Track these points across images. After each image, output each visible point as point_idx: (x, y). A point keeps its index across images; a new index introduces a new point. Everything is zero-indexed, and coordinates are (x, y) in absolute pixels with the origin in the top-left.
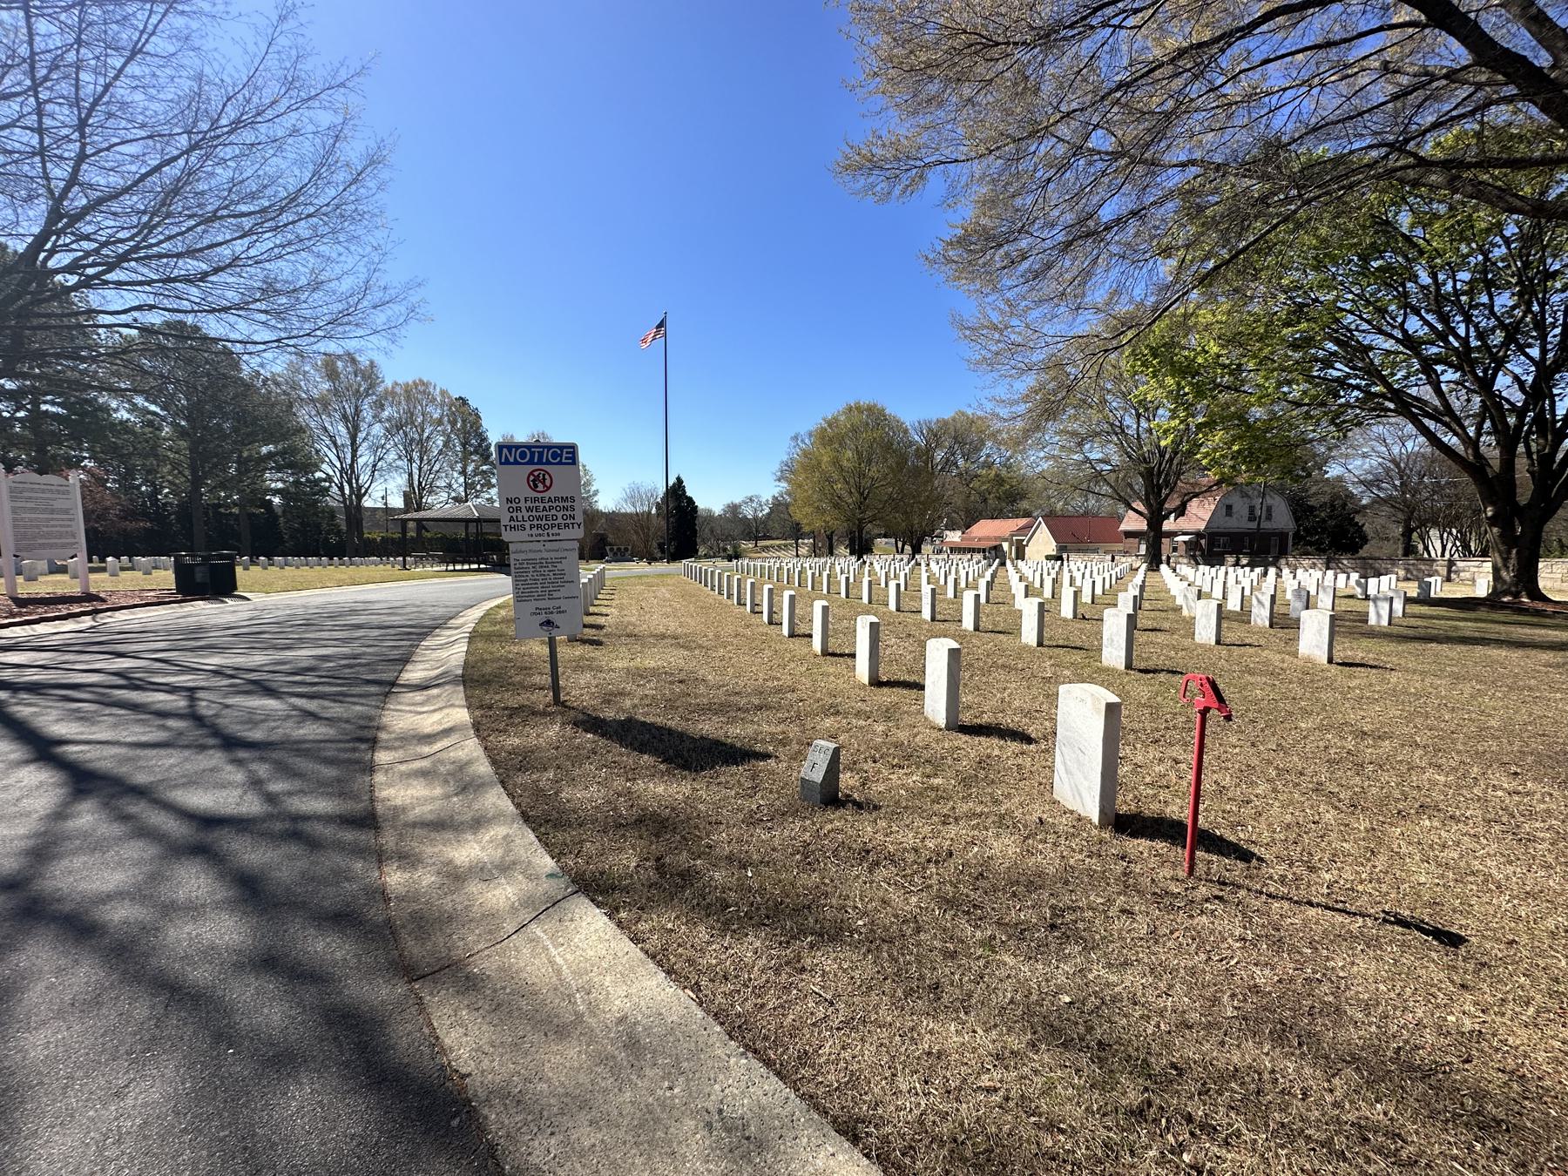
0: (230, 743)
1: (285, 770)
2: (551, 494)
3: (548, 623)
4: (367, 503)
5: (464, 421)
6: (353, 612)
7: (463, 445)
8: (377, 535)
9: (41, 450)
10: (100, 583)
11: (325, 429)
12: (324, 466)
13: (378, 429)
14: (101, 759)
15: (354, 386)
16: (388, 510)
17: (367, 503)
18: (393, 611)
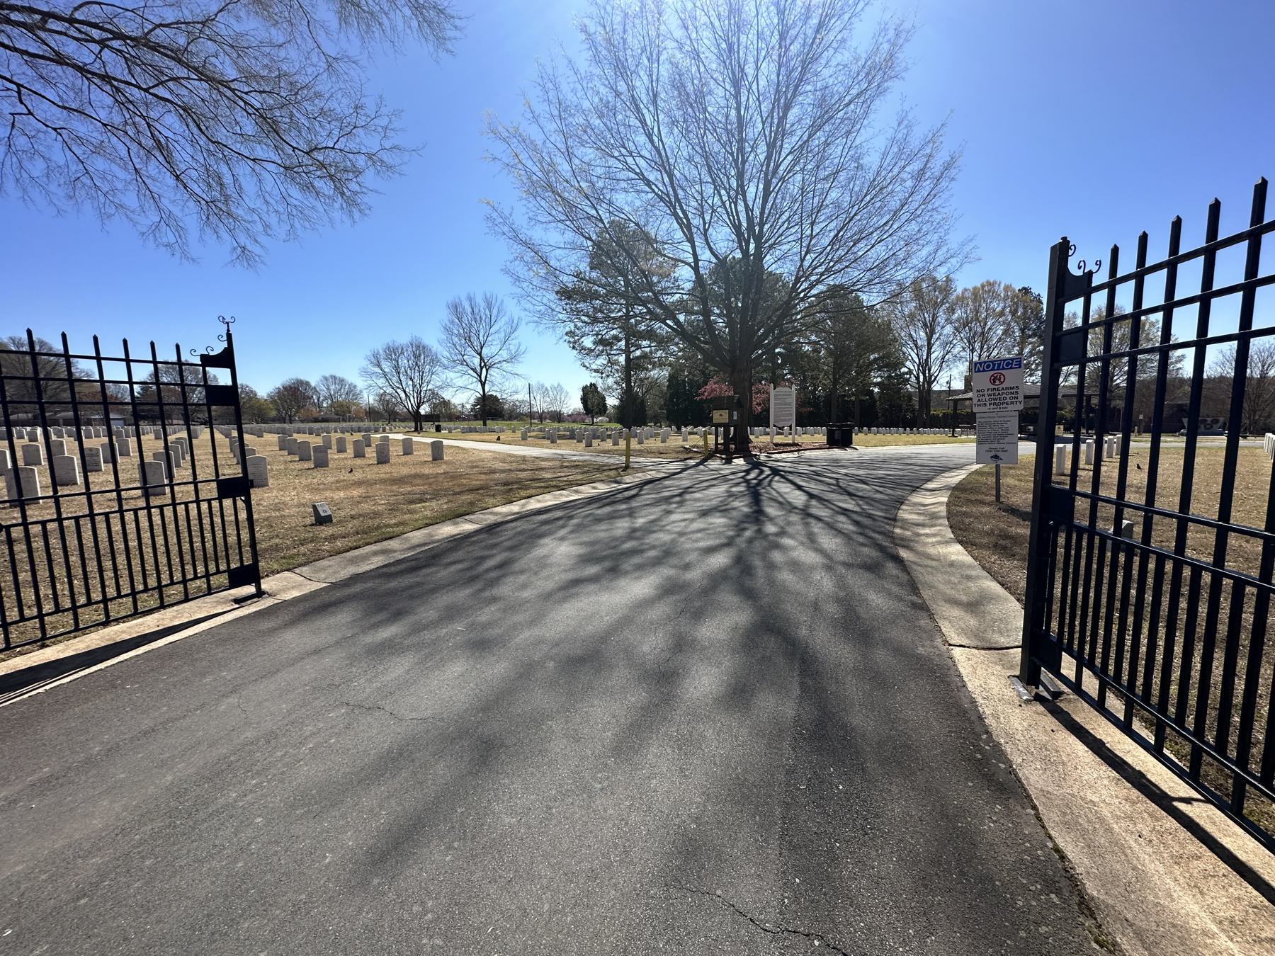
0: (850, 494)
1: (868, 504)
2: (1003, 386)
3: (996, 457)
4: (936, 387)
5: (1025, 308)
6: (910, 458)
7: (1022, 330)
8: (939, 412)
9: (774, 373)
10: (798, 439)
11: (911, 336)
12: (908, 364)
13: (949, 329)
14: (815, 492)
15: (930, 296)
16: (950, 392)
17: (936, 387)
18: (932, 459)
